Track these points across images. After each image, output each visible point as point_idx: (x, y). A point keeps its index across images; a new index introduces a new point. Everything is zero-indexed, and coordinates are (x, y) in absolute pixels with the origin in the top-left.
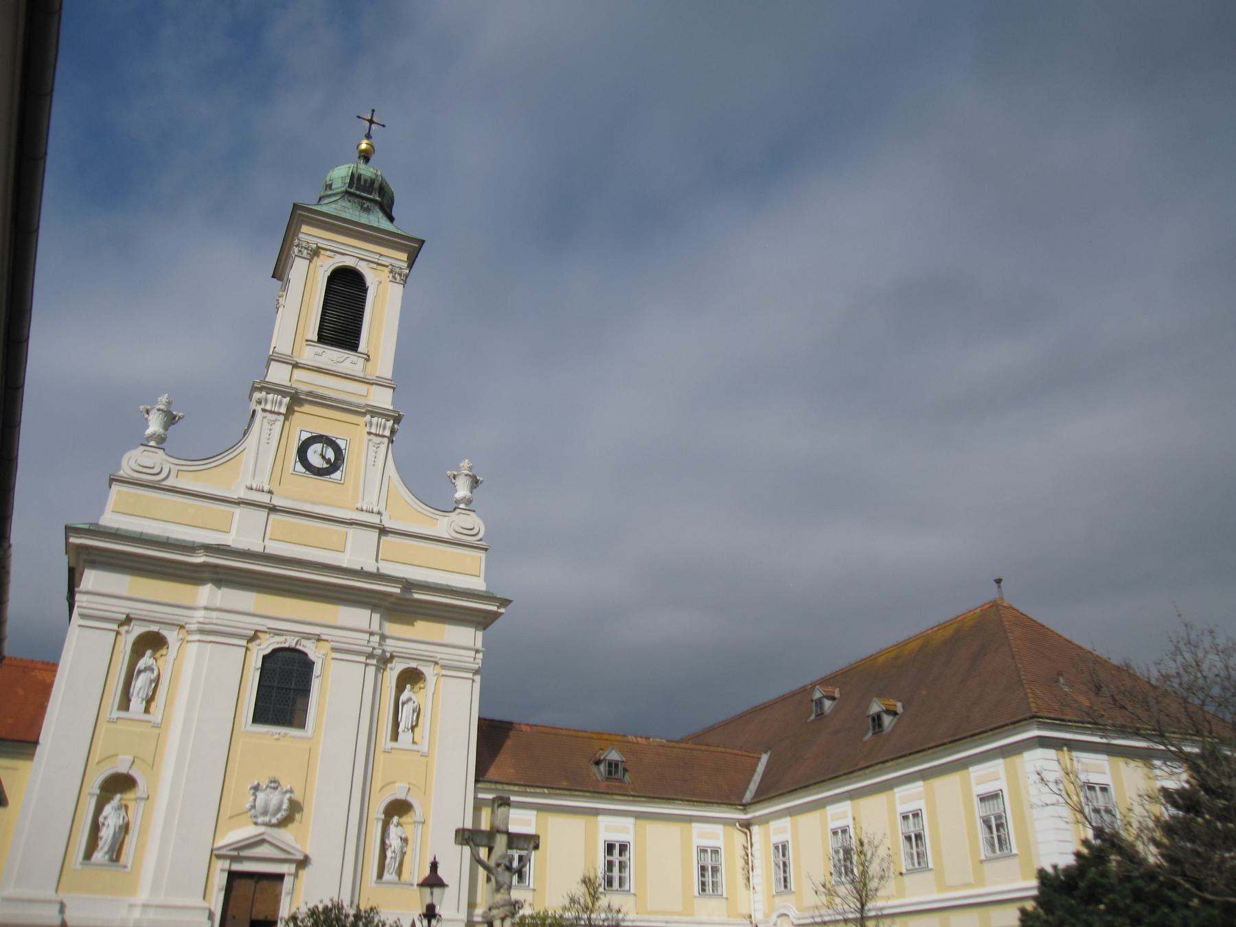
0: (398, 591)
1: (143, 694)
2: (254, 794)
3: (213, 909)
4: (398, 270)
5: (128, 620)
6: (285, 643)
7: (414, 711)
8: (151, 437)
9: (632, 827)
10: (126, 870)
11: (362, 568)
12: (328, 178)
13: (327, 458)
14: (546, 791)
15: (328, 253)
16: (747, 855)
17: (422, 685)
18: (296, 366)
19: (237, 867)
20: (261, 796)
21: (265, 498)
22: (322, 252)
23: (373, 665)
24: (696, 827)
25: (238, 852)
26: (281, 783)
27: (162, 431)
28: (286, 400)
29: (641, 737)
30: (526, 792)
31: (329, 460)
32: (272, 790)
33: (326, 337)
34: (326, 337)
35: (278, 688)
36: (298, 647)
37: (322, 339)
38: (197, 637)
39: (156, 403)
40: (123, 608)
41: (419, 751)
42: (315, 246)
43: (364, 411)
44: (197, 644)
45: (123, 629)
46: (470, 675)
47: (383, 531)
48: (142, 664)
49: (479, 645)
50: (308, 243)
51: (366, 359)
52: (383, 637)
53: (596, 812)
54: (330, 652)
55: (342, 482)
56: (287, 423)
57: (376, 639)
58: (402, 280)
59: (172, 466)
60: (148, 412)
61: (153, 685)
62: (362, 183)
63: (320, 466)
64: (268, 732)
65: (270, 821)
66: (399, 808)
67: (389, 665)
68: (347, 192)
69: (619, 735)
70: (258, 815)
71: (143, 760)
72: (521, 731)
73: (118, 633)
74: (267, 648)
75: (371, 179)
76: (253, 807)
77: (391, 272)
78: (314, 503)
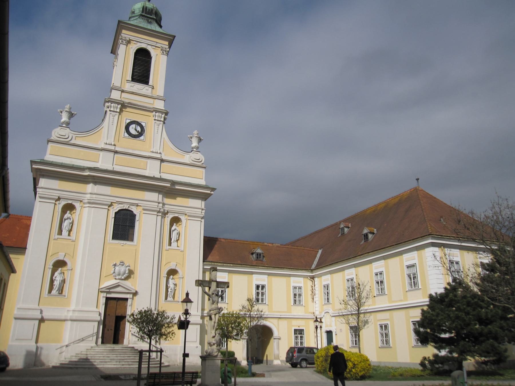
0: (169, 185)
1: (67, 229)
2: (114, 267)
4: (164, 49)
5: (59, 199)
6: (124, 207)
7: (177, 234)
8: (63, 123)
9: (227, 276)
10: (65, 297)
11: (154, 176)
14: (232, 265)
15: (134, 42)
16: (313, 290)
17: (180, 224)
18: (123, 91)
19: (109, 296)
20: (117, 268)
21: (112, 148)
22: (132, 42)
23: (160, 216)
25: (109, 290)
26: (125, 263)
29: (270, 243)
31: (139, 131)
32: (121, 266)
33: (135, 79)
34: (135, 79)
36: (129, 209)
38: (88, 205)
39: (65, 108)
40: (56, 194)
41: (71, 239)
43: (152, 110)
44: (88, 208)
45: (57, 202)
47: (162, 161)
48: (66, 216)
49: (203, 207)
50: (125, 38)
51: (152, 88)
55: (144, 140)
57: (161, 205)
59: (73, 135)
60: (61, 112)
61: (71, 225)
62: (148, 11)
64: (119, 243)
66: (172, 272)
68: (141, 15)
69: (261, 243)
73: (55, 204)
76: (114, 272)
77: (162, 50)
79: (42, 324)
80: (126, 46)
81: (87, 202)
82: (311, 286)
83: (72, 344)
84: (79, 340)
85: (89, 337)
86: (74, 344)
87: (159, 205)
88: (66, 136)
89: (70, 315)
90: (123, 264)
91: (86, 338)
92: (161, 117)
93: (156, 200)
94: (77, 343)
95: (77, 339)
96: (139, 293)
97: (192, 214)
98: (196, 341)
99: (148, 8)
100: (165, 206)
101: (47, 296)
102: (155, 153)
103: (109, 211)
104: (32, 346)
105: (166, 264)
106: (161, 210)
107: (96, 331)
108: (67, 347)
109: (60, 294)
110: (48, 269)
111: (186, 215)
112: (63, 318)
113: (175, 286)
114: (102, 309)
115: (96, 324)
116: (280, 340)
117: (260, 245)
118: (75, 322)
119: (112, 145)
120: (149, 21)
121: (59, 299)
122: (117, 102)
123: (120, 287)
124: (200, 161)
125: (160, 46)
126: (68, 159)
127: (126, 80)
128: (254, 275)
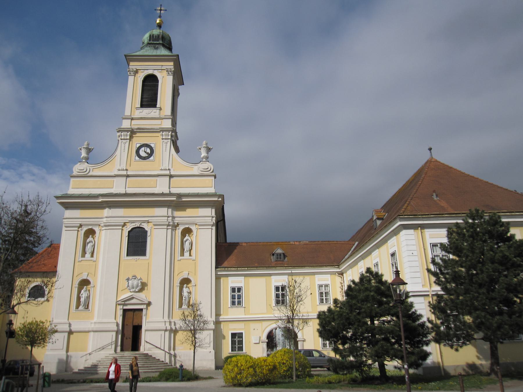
0: (175, 199)
1: (90, 251)
2: (128, 281)
3: (118, 322)
4: (169, 70)
5: (81, 226)
6: (136, 225)
7: (190, 244)
8: (203, 158)
9: (329, 278)
10: (90, 311)
11: (163, 192)
12: (143, 40)
13: (147, 152)
14: (246, 268)
16: (342, 286)
17: (192, 234)
18: (132, 119)
19: (125, 307)
20: (130, 282)
21: (124, 173)
22: (139, 71)
23: (170, 229)
24: (317, 277)
25: (124, 302)
26: (137, 276)
27: (206, 155)
28: (129, 133)
29: (297, 242)
30: (238, 270)
31: (148, 152)
32: (134, 280)
35: (141, 242)
36: (141, 226)
37: (142, 106)
38: (105, 228)
39: (202, 145)
40: (79, 221)
41: (92, 260)
42: (135, 69)
43: (159, 130)
44: (105, 230)
45: (80, 229)
46: (210, 227)
47: (171, 176)
48: (88, 241)
49: (214, 214)
50: (133, 69)
51: (160, 110)
52: (173, 217)
53: (270, 275)
54: (153, 226)
55: (154, 160)
56: (131, 142)
57: (171, 218)
58: (172, 73)
59: (90, 167)
60: (200, 149)
61: (93, 247)
63: (145, 156)
64: (132, 259)
65: (135, 290)
66: (186, 281)
67: (177, 228)
68: (148, 44)
69: (286, 242)
70: (131, 289)
71: (90, 273)
72: (242, 246)
73: (78, 231)
74: (129, 228)
75: (158, 35)
76: (128, 286)
77: (167, 71)
78: (143, 171)
79: (71, 336)
80: (134, 76)
81: (103, 225)
82: (340, 282)
83: (94, 352)
84: (99, 348)
85: (108, 345)
86: (96, 352)
87: (169, 219)
88: (85, 169)
89: (92, 327)
90: (135, 277)
91: (106, 346)
92: (168, 135)
93: (166, 215)
94: (99, 351)
95: (99, 348)
96: (152, 304)
97: (207, 223)
98: (62, 348)
99: (154, 35)
100: (175, 219)
101: (74, 311)
102: (164, 170)
103: (123, 231)
104: (63, 354)
105: (178, 274)
106: (171, 223)
107: (114, 339)
108: (90, 355)
109: (86, 309)
110: (75, 288)
111: (196, 224)
112: (87, 330)
113: (357, 291)
114: (120, 320)
115: (114, 334)
116: (304, 342)
117: (284, 245)
118: (96, 333)
119: (167, 170)
120: (156, 47)
121: (85, 313)
122: (126, 130)
123: (134, 299)
124: (89, 170)
125: (165, 68)
126: (87, 190)
127: (135, 109)
128: (272, 277)
